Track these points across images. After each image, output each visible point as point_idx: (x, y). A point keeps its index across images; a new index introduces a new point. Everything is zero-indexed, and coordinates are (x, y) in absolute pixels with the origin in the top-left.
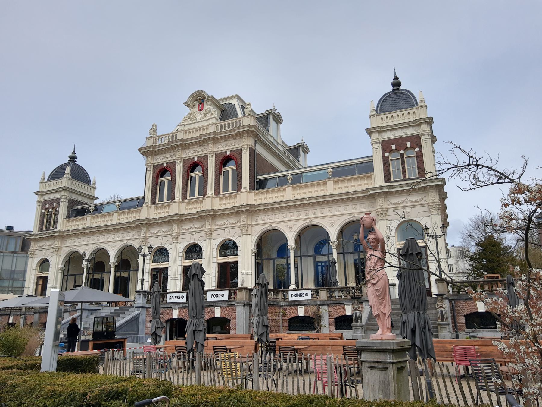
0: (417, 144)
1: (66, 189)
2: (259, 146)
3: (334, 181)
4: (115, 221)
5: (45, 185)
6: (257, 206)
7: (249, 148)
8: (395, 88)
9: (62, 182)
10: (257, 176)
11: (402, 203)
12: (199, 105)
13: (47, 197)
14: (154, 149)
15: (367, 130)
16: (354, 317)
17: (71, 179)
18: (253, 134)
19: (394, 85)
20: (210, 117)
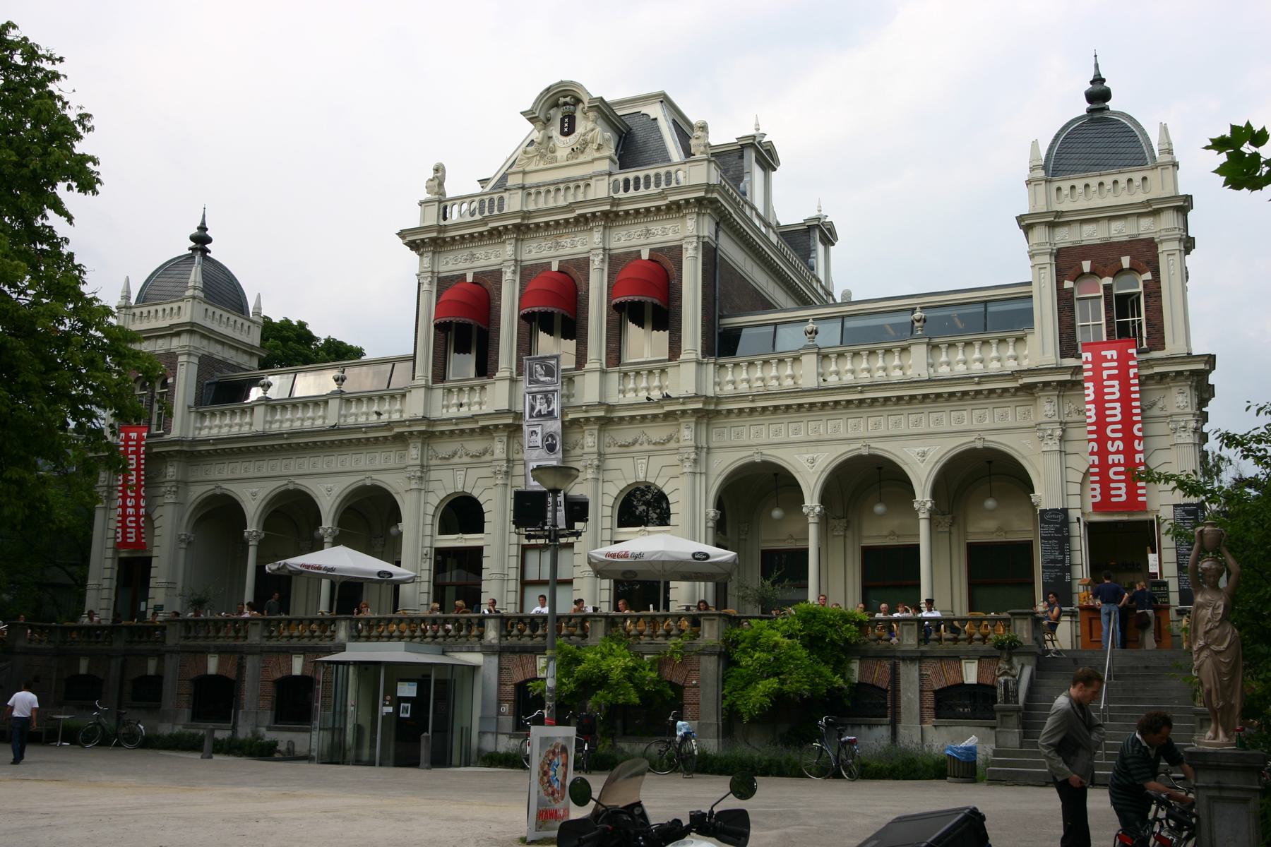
0: (1148, 263)
1: (192, 329)
3: (928, 344)
6: (725, 400)
7: (704, 243)
8: (1095, 106)
9: (179, 308)
10: (721, 317)
12: (562, 121)
14: (442, 236)
15: (1020, 219)
16: (1001, 691)
17: (205, 302)
18: (714, 206)
19: (1090, 97)
20: (597, 155)
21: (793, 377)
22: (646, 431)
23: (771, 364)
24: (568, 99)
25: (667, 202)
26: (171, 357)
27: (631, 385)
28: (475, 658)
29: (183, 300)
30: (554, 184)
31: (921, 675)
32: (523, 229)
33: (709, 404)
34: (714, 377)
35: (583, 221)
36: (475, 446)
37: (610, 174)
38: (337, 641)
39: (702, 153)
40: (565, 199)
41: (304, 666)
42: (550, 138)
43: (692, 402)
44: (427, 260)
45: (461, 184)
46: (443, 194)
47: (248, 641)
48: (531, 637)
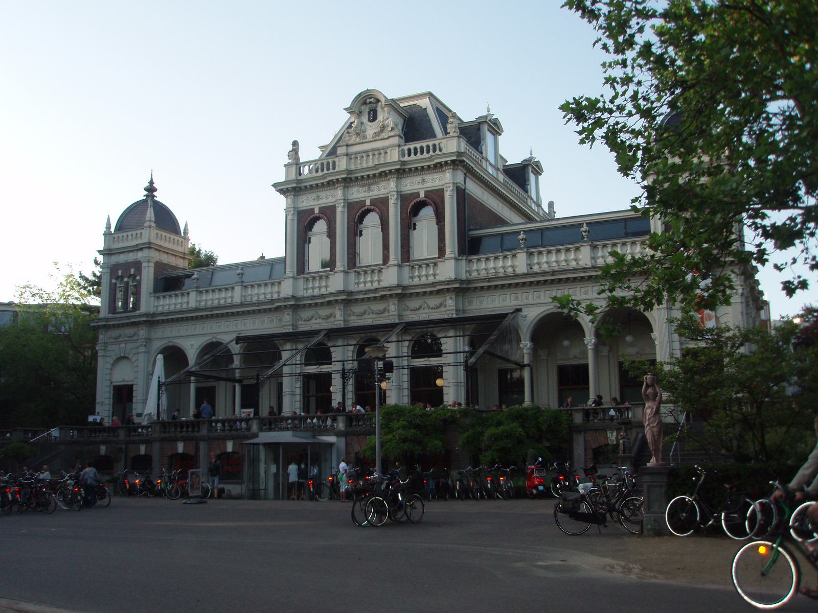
2: (470, 181)
3: (591, 246)
4: (522, 268)
5: (112, 239)
9: (141, 233)
10: (469, 230)
11: (134, 336)
12: (369, 113)
13: (122, 258)
21: (576, 260)
22: (426, 300)
23: (499, 259)
24: (372, 100)
25: (434, 163)
26: (138, 265)
27: (310, 286)
28: (332, 439)
29: (143, 229)
30: (383, 149)
31: (585, 441)
32: (348, 180)
33: (464, 284)
34: (466, 267)
35: (384, 175)
36: (129, 331)
37: (399, 146)
38: (252, 432)
39: (454, 132)
40: (373, 162)
41: (234, 446)
42: (362, 123)
43: (453, 284)
44: (289, 201)
45: (310, 153)
46: (298, 159)
47: (201, 433)
48: (187, 431)
